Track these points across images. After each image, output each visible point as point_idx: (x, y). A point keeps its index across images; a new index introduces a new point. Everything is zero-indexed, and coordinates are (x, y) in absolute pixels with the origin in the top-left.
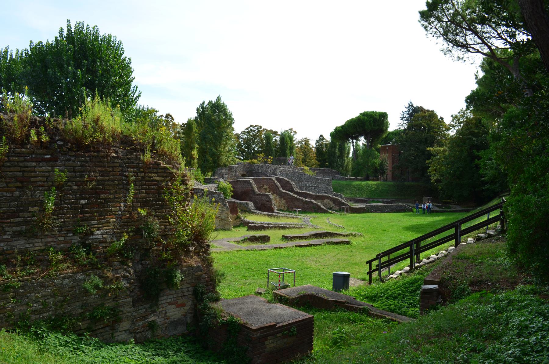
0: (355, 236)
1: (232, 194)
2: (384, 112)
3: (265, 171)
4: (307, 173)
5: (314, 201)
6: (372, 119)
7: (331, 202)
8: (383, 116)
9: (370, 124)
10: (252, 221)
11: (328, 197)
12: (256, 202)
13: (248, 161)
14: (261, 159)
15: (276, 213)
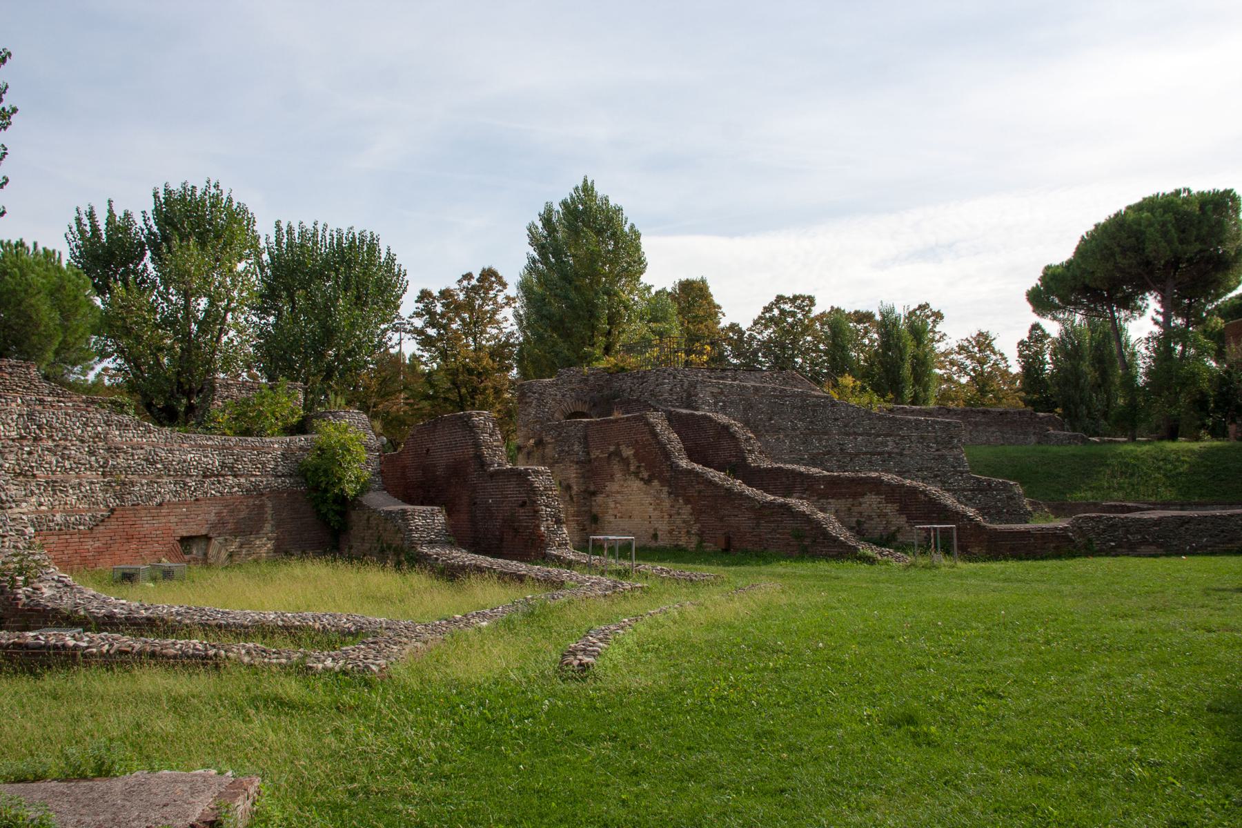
3: (653, 394)
4: (853, 401)
5: (802, 505)
6: (1169, 217)
7: (890, 509)
11: (876, 486)
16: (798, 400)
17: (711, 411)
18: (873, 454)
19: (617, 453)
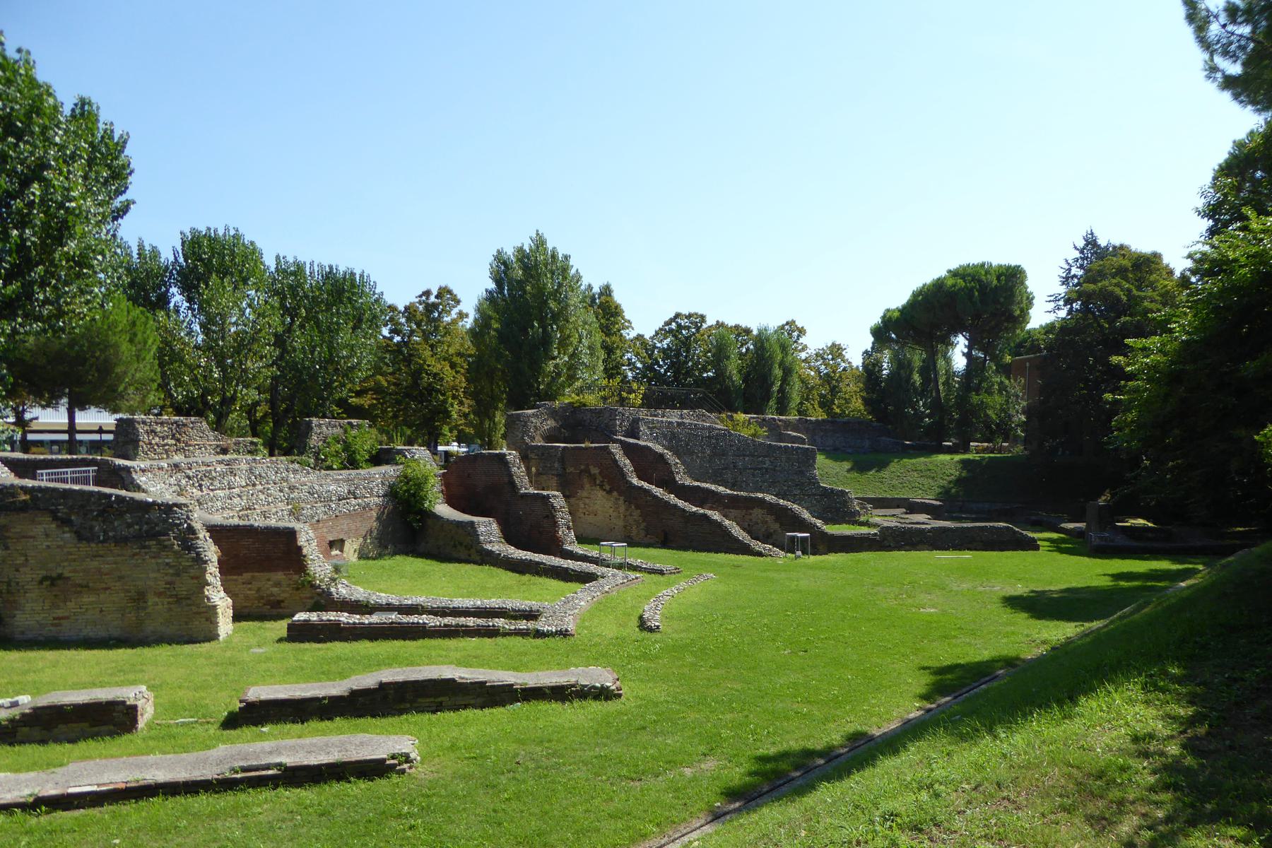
2: (1013, 264)
3: (607, 425)
5: (715, 516)
7: (769, 518)
8: (1012, 278)
9: (978, 300)
17: (650, 441)
19: (587, 471)
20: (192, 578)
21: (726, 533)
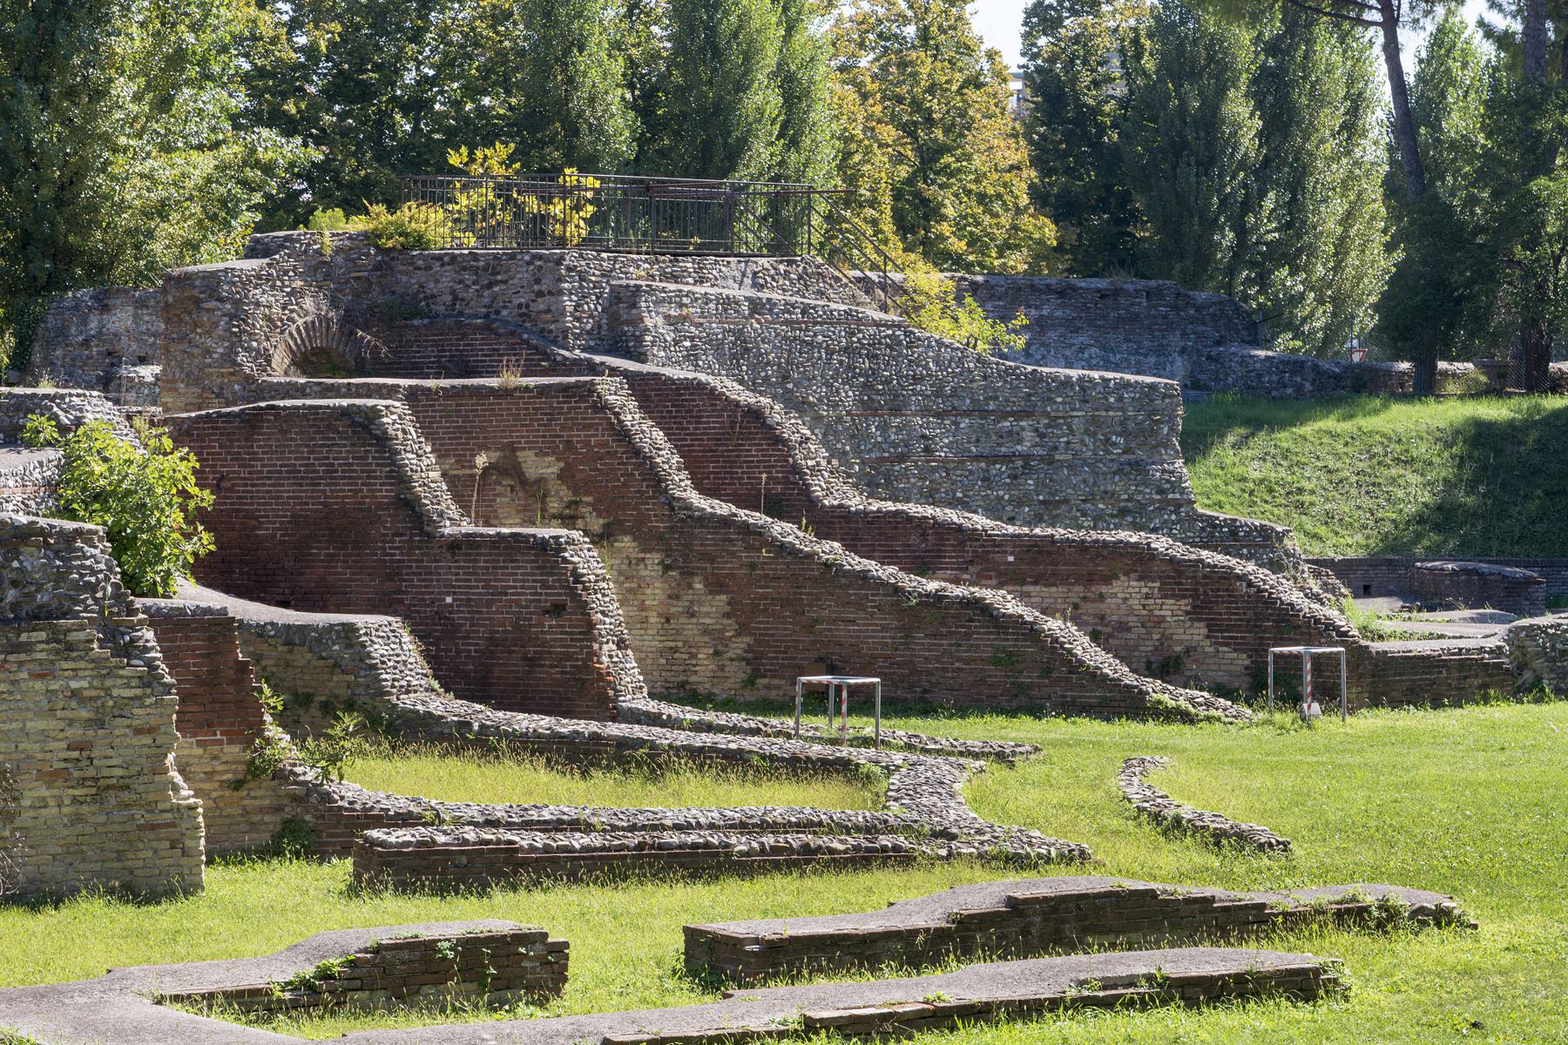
0: (1386, 920)
1: (205, 541)
3: (525, 314)
5: (1007, 603)
7: (1171, 610)
10: (400, 804)
11: (1140, 561)
12: (443, 615)
13: (359, 224)
14: (484, 195)
15: (635, 717)
16: (840, 330)
18: (993, 459)
20: (138, 731)
21: (1057, 658)
